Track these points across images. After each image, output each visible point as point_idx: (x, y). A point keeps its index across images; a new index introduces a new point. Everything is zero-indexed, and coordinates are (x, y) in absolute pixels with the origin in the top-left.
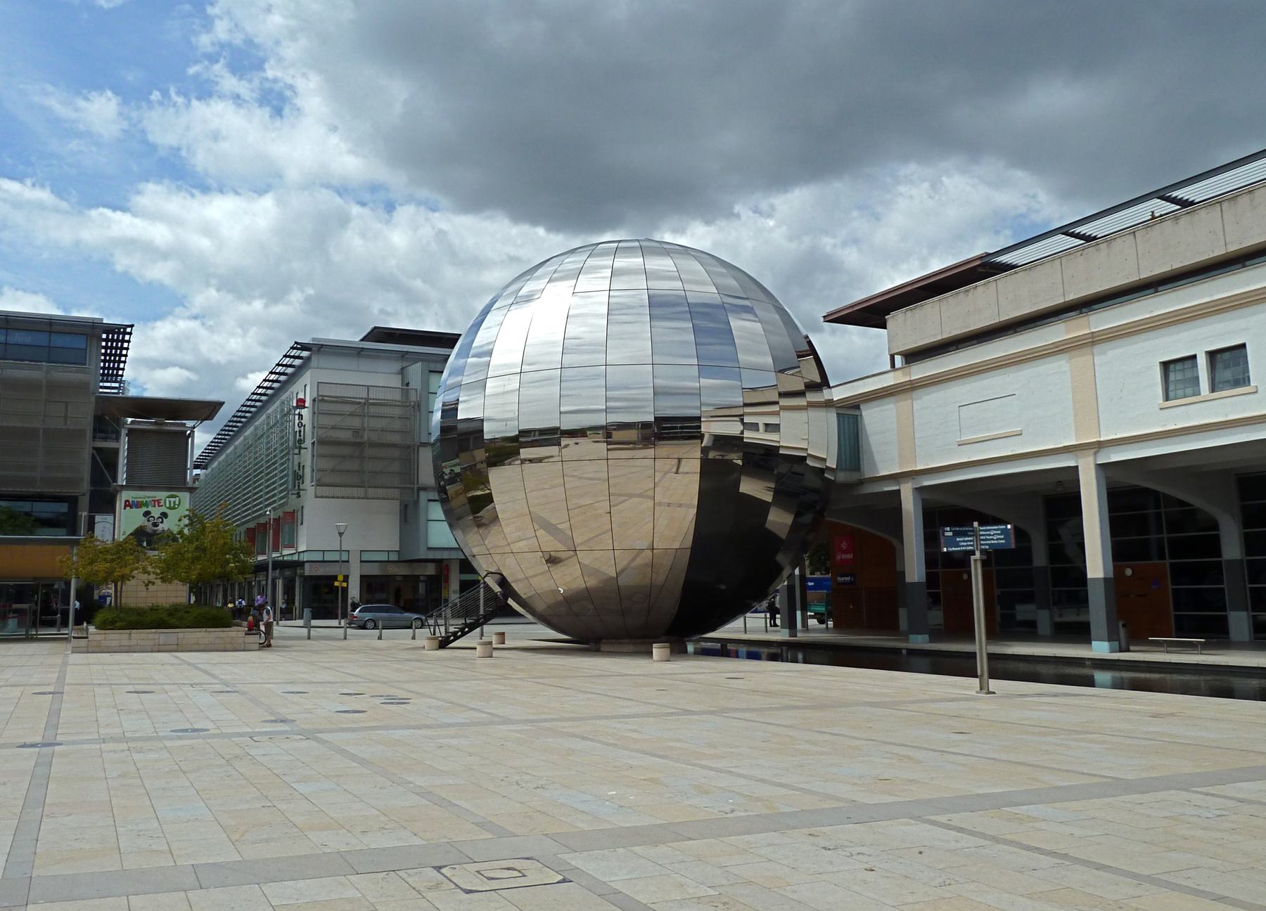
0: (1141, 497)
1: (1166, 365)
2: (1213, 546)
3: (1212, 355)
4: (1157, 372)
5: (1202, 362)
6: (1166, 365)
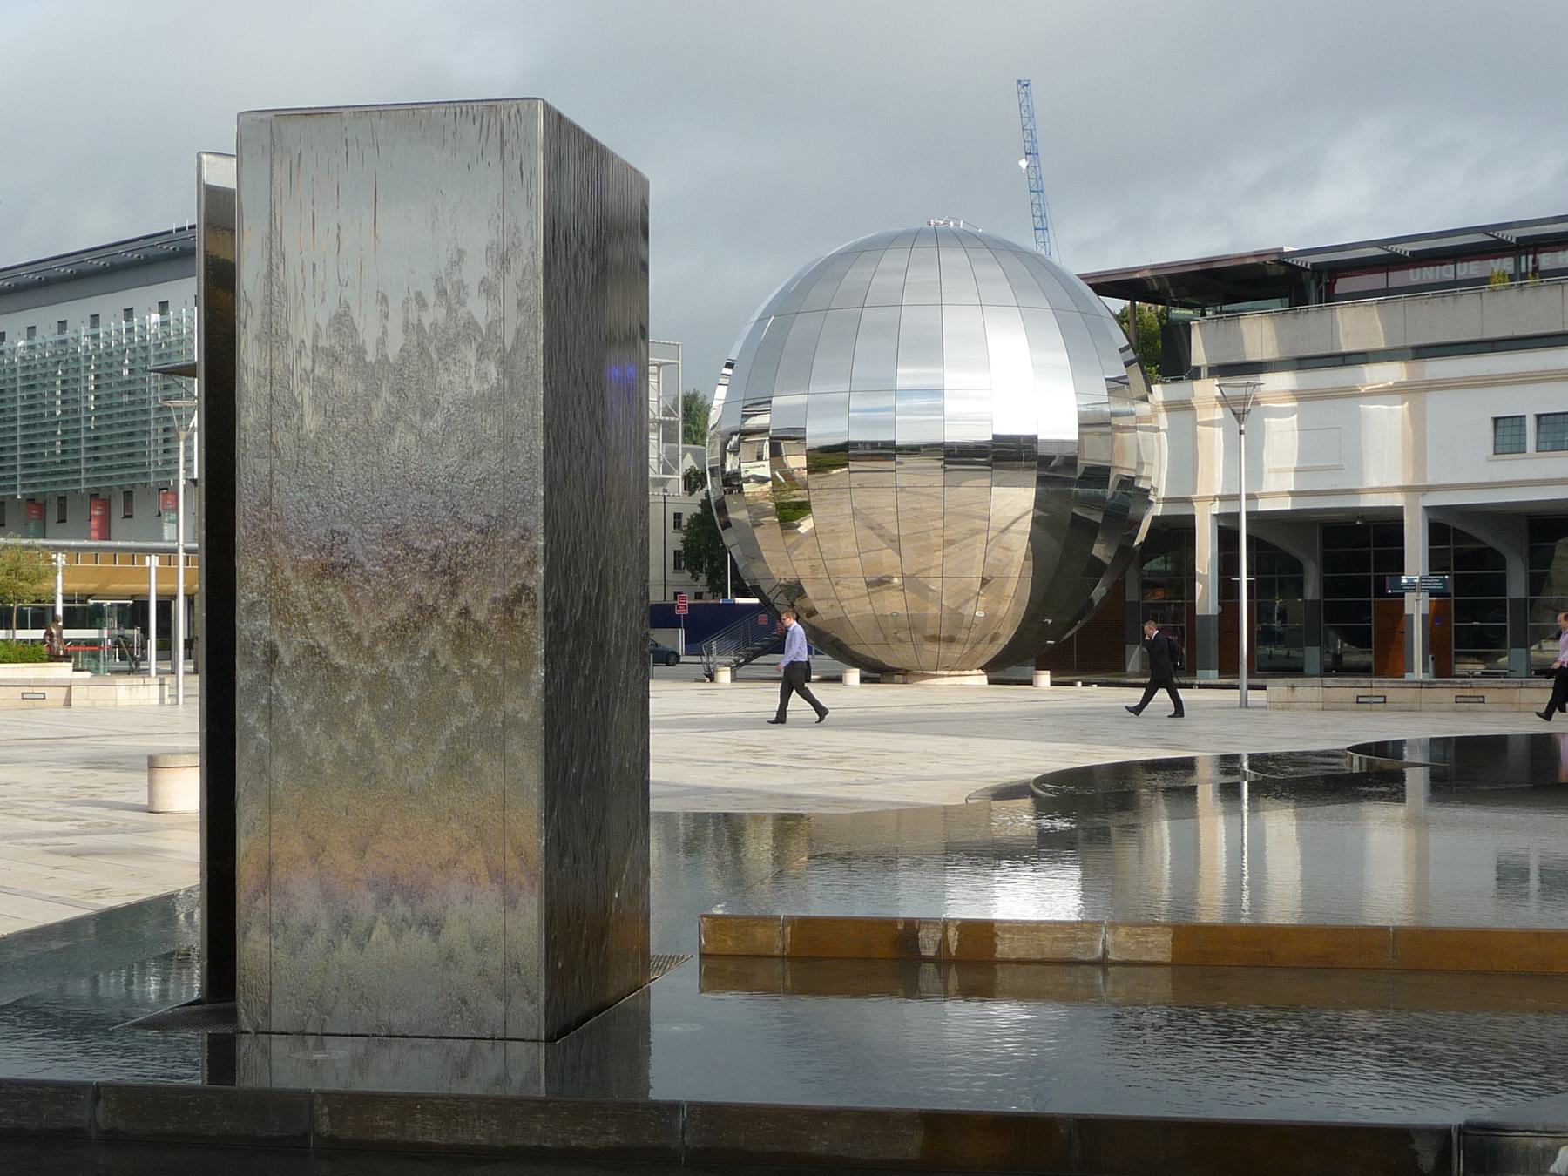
0: (1464, 539)
1: (1496, 420)
2: (1500, 585)
3: (1539, 417)
4: (1490, 425)
5: (1531, 424)
6: (1496, 420)
